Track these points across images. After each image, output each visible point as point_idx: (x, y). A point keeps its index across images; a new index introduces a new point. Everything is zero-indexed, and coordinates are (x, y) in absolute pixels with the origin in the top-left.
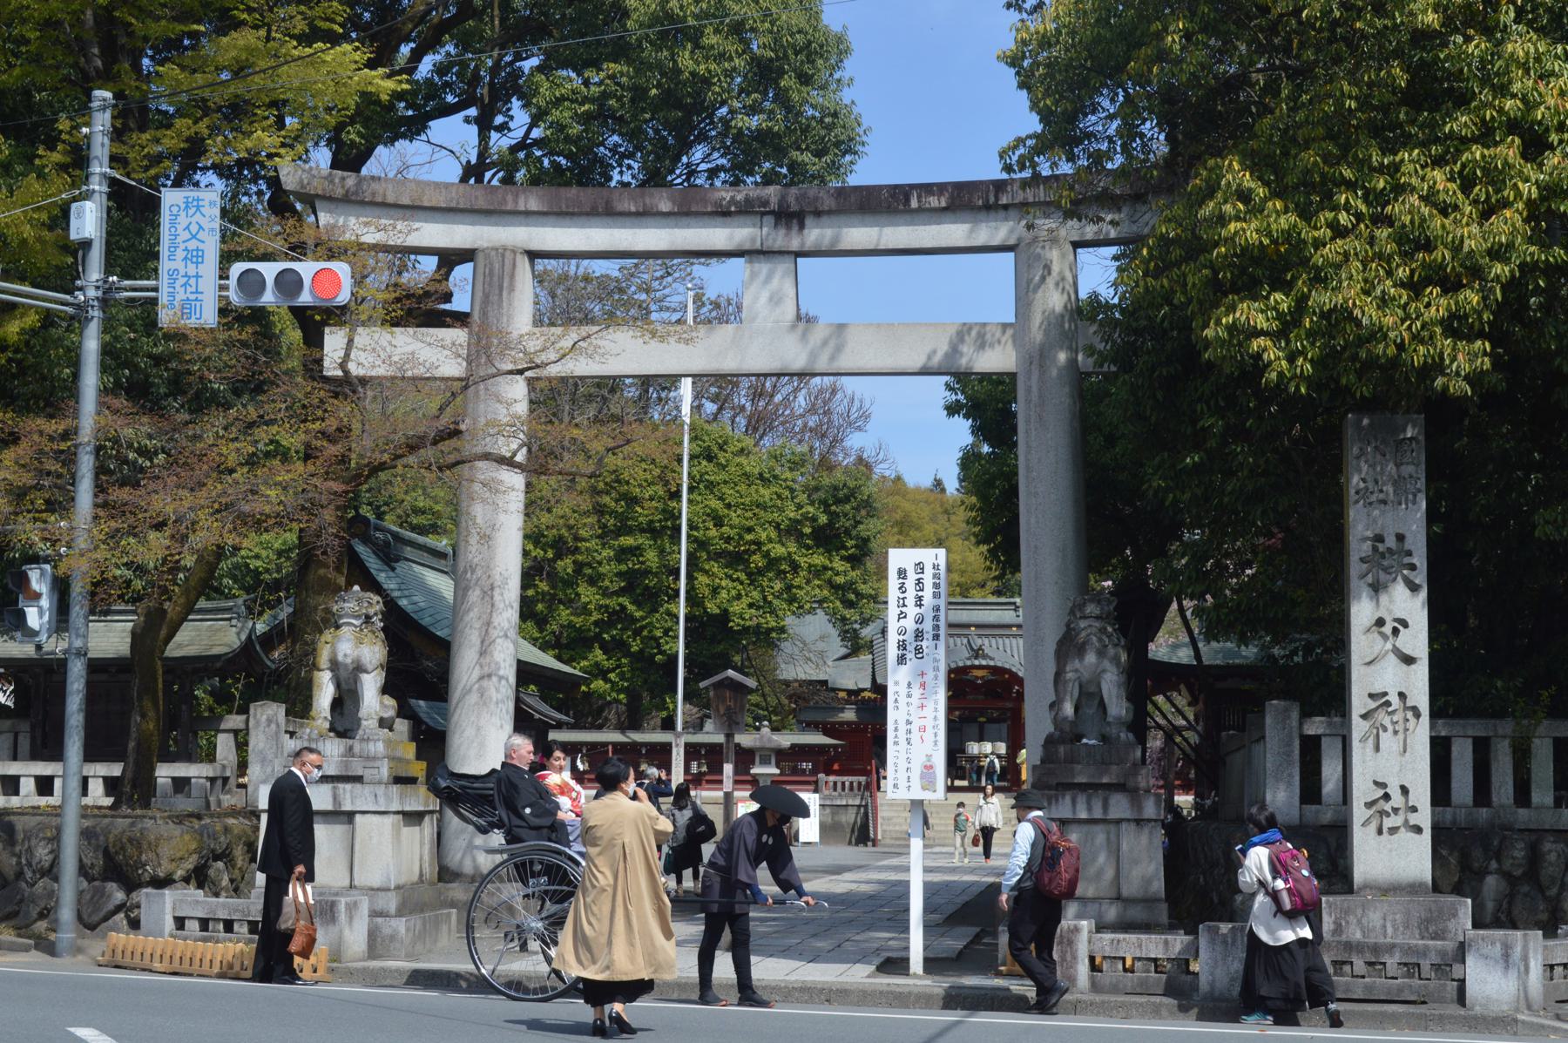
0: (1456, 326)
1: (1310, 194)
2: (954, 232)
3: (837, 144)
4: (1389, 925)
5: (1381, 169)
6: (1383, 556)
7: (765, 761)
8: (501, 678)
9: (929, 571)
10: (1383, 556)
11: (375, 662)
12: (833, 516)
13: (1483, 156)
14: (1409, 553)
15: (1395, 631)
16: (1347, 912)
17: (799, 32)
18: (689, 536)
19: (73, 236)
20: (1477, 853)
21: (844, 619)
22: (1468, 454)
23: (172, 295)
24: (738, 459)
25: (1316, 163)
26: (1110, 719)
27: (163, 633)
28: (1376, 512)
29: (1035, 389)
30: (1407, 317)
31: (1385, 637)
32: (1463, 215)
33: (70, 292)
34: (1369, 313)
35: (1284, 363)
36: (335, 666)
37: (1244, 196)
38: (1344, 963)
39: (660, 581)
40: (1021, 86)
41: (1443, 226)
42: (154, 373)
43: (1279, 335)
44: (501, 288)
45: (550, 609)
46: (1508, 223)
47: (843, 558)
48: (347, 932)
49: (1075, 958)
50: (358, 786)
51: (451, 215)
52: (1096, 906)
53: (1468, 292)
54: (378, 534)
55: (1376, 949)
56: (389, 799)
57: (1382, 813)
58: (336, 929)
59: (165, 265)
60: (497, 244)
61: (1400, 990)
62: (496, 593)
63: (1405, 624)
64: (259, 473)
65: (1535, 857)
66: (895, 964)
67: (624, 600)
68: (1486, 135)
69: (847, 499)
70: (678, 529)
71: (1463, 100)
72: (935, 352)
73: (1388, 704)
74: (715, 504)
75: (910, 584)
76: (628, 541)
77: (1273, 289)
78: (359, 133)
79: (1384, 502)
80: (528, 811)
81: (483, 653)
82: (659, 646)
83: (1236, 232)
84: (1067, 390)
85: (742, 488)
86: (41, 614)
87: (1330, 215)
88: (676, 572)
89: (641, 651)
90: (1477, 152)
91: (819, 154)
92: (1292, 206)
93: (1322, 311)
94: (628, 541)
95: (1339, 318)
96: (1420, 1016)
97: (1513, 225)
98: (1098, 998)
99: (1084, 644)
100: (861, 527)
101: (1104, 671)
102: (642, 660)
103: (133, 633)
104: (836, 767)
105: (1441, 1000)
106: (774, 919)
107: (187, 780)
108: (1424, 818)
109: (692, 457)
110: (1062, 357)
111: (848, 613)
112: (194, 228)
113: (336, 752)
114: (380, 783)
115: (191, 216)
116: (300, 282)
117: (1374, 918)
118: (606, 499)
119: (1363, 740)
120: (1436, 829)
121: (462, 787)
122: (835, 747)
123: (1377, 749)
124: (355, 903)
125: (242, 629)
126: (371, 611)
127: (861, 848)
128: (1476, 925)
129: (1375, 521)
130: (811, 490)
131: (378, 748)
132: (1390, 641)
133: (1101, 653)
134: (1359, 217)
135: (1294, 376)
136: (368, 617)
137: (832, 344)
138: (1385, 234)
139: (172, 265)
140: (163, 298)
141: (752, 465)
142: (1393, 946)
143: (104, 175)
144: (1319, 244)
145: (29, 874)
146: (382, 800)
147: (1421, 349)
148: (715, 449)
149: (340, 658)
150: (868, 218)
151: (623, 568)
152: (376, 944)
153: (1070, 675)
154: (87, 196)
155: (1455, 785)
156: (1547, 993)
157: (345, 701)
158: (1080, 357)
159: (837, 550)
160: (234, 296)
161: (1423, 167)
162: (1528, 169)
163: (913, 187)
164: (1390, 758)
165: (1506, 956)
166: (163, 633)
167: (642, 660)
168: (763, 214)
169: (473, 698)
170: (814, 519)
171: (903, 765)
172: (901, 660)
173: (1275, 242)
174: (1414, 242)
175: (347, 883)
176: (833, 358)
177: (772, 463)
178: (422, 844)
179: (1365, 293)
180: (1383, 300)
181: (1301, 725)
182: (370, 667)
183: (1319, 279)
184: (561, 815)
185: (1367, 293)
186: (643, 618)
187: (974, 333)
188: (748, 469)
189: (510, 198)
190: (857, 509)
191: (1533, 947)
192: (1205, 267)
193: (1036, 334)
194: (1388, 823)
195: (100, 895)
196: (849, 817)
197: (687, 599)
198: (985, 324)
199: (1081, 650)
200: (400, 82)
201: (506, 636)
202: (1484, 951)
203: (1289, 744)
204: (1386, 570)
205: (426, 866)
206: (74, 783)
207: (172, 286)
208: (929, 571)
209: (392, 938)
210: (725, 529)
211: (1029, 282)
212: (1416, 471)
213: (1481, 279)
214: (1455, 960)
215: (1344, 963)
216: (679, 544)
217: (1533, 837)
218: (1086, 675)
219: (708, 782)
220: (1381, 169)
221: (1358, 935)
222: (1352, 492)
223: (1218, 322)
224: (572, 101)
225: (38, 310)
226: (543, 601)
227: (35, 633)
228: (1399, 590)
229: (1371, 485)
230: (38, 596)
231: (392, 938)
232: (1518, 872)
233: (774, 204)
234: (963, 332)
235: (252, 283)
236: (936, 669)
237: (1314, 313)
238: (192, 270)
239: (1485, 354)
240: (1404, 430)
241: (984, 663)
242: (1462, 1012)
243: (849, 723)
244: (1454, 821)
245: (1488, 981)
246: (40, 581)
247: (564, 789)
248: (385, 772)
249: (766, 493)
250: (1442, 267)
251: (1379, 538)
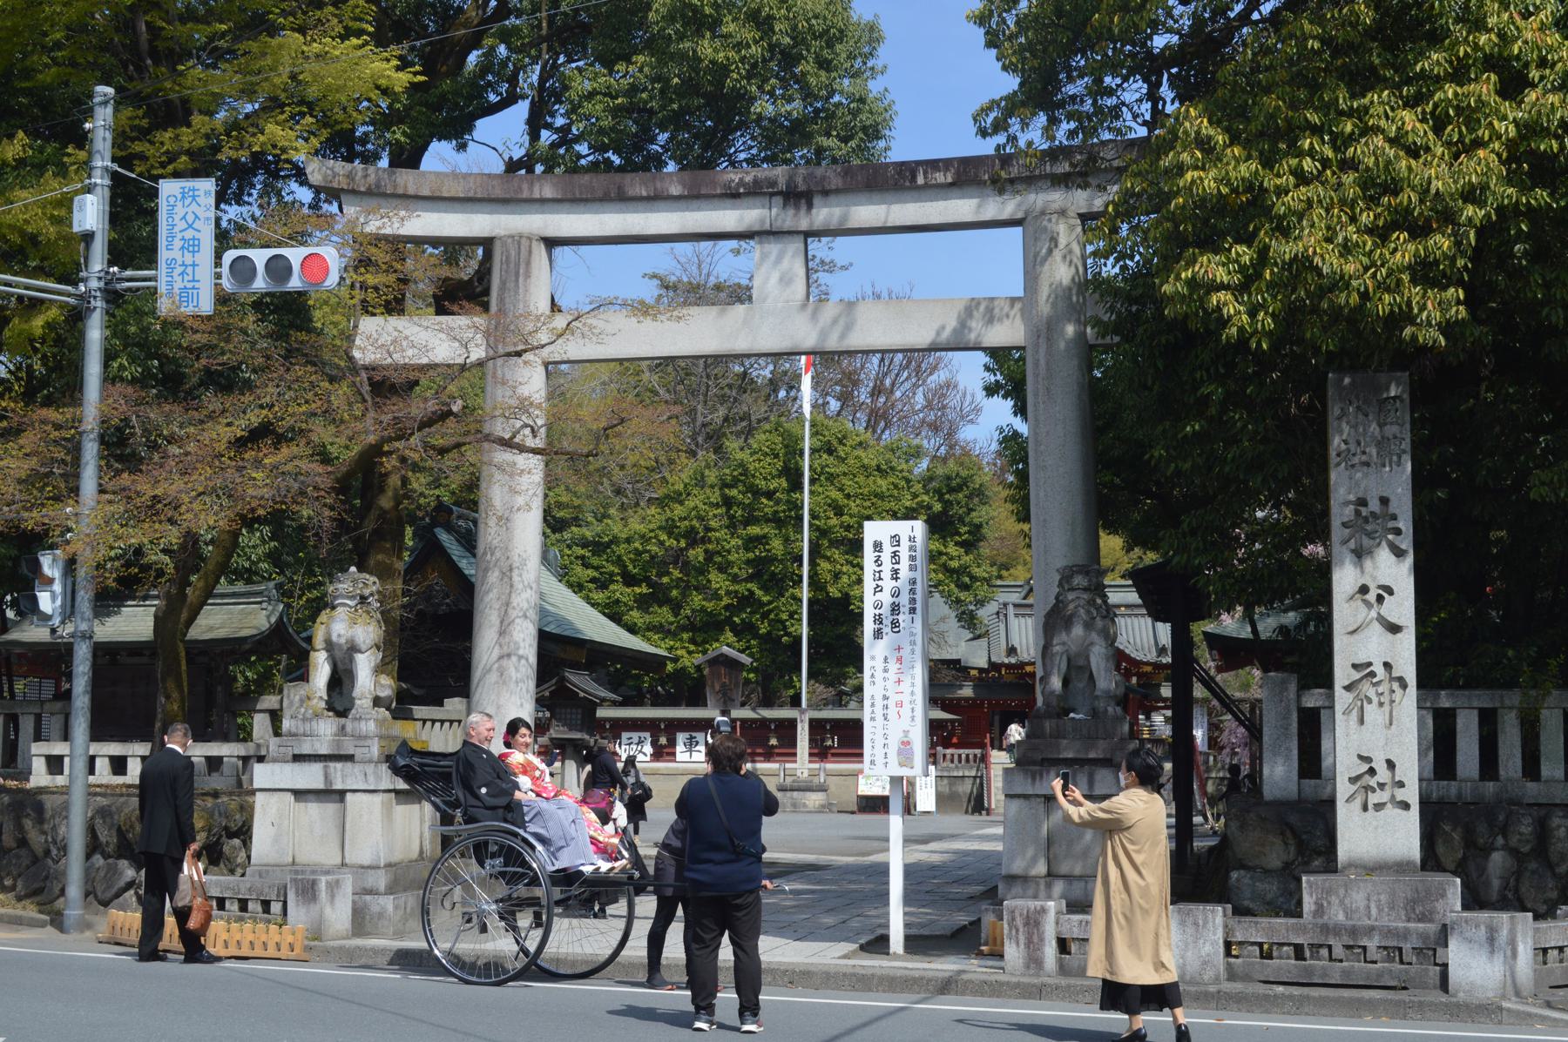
0: (1426, 272)
1: (1271, 142)
2: (962, 207)
3: (864, 129)
4: (1373, 905)
5: (1350, 113)
6: (1366, 520)
8: (520, 657)
9: (905, 544)
10: (1366, 520)
11: (369, 642)
12: (948, 505)
13: (1456, 94)
14: (1394, 517)
15: (1380, 599)
16: (1329, 892)
17: (816, 17)
18: (811, 525)
19: (76, 229)
20: (1482, 828)
21: (958, 601)
22: (1453, 410)
23: (170, 283)
24: (856, 453)
25: (1278, 108)
26: (1097, 693)
27: (184, 615)
28: (1359, 475)
29: (1042, 362)
30: (1373, 264)
31: (1368, 605)
32: (1434, 156)
33: (75, 284)
34: (1330, 262)
35: (1245, 317)
36: (330, 646)
37: (1204, 144)
38: (1321, 946)
39: (785, 567)
40: (990, 44)
41: (1410, 168)
42: (168, 366)
43: (1240, 290)
44: (517, 274)
45: (684, 595)
46: (1485, 163)
47: (956, 544)
48: (328, 910)
49: (1042, 940)
50: (349, 765)
51: (469, 205)
52: (1082, 884)
53: (1438, 237)
54: (460, 523)
55: (1354, 931)
56: (378, 778)
57: (1368, 789)
58: (317, 907)
59: (163, 255)
60: (513, 232)
61: (1380, 975)
62: (515, 573)
63: (1390, 591)
64: (246, 456)
65: (1543, 833)
66: (879, 944)
67: (753, 586)
68: (1459, 74)
69: (959, 488)
70: (801, 518)
71: (1436, 38)
72: (943, 328)
73: (1372, 674)
74: (835, 494)
75: (886, 556)
76: (755, 530)
77: (1238, 241)
78: (404, 133)
79: (1367, 464)
80: (484, 790)
81: (502, 633)
82: (785, 628)
83: (1193, 182)
84: (1075, 362)
85: (861, 479)
86: (53, 600)
87: (1294, 162)
88: (799, 559)
89: (769, 633)
90: (1450, 90)
91: (845, 140)
92: (1255, 154)
93: (1283, 261)
94: (755, 530)
95: (1302, 265)
96: (1398, 1003)
97: (1487, 165)
98: (1063, 981)
99: (1071, 616)
100: (974, 514)
101: (1092, 644)
102: (770, 642)
103: (156, 617)
104: (955, 740)
105: (1424, 986)
106: (813, 892)
108: (1411, 794)
109: (813, 451)
110: (1070, 330)
111: (962, 595)
112: (190, 218)
113: (329, 732)
114: (370, 761)
115: (186, 207)
116: (289, 269)
117: (1358, 898)
118: (734, 492)
119: (1347, 712)
120: (1424, 802)
121: (421, 765)
122: (952, 721)
123: (1362, 721)
124: (337, 882)
125: (272, 612)
126: (367, 592)
127: (976, 817)
128: (1465, 907)
129: (1357, 484)
130: (928, 479)
131: (370, 727)
132: (1375, 608)
133: (1088, 626)
134: (1326, 163)
135: (1256, 331)
136: (363, 599)
137: (842, 322)
138: (1351, 178)
139: (171, 255)
140: (162, 288)
141: (870, 458)
142: (1372, 929)
143: (106, 169)
144: (1281, 191)
145: (54, 852)
146: (371, 778)
147: (1387, 298)
148: (835, 443)
149: (334, 638)
150: (876, 196)
151: (751, 555)
152: (361, 921)
153: (1057, 649)
154: (89, 190)
155: (1460, 758)
156: (1538, 978)
157: (340, 681)
158: (1089, 330)
159: (952, 535)
160: (227, 284)
161: (1393, 109)
162: (1506, 107)
163: (919, 163)
164: (1378, 735)
165: (1491, 940)
166: (184, 615)
167: (770, 642)
168: (772, 195)
169: (493, 677)
170: (929, 507)
171: (880, 741)
172: (878, 634)
173: (1235, 191)
174: (1379, 186)
175: (338, 861)
176: (843, 336)
177: (889, 455)
178: (422, 821)
179: (1326, 239)
180: (1345, 246)
181: (1299, 697)
182: (363, 647)
183: (1283, 230)
184: (518, 795)
185: (1329, 240)
186: (770, 603)
187: (982, 308)
188: (866, 461)
189: (525, 186)
190: (970, 497)
191: (1522, 931)
192: (1168, 220)
193: (1044, 307)
194: (1374, 798)
195: (113, 872)
196: (966, 788)
197: (810, 585)
198: (992, 299)
199: (1068, 623)
200: (415, 74)
201: (525, 616)
202: (1467, 935)
203: (1286, 717)
204: (1370, 535)
205: (427, 844)
206: (81, 765)
207: (170, 275)
208: (905, 544)
209: (381, 915)
210: (845, 518)
211: (1036, 255)
212: (1401, 431)
213: (1454, 224)
214: (1437, 943)
215: (1321, 946)
216: (802, 532)
217: (1543, 812)
218: (1074, 648)
219: (833, 755)
220: (1350, 113)
221: (1341, 917)
222: (1333, 453)
223: (1178, 278)
224: (605, 95)
225: (63, 306)
226: (677, 587)
227: (48, 618)
228: (1384, 556)
229: (1353, 447)
230: (51, 581)
231: (381, 915)
232: (1526, 849)
233: (782, 185)
234: (971, 308)
235: (243, 270)
236: (913, 643)
237: (1276, 264)
238: (189, 259)
239: (1459, 302)
240: (1388, 389)
242: (1444, 999)
243: (967, 699)
244: (1459, 796)
245: (1472, 966)
246: (51, 567)
247: (527, 769)
248: (375, 751)
249: (883, 484)
250: (1408, 211)
251: (1362, 502)
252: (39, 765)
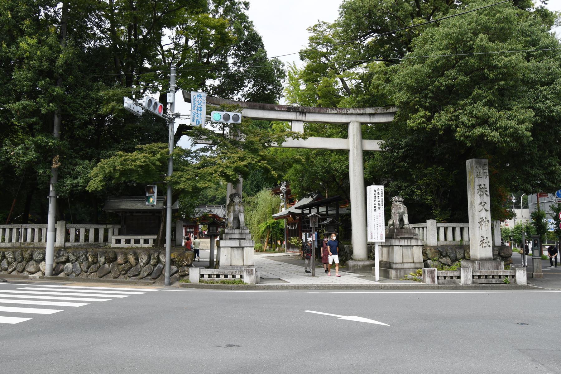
9: (380, 191)
107: (117, 243)
112: (200, 102)
175: (242, 264)
194: (484, 245)
208: (380, 191)
238: (199, 112)
252: (151, 242)
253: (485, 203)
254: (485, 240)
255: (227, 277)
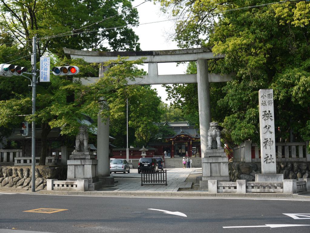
7: (144, 153)
15: (269, 127)
65: (292, 165)
108: (275, 160)
112: (46, 64)
123: (266, 148)
175: (210, 175)
238: (45, 71)
241: (183, 134)
253: (270, 126)
254: (270, 157)
255: (68, 186)
